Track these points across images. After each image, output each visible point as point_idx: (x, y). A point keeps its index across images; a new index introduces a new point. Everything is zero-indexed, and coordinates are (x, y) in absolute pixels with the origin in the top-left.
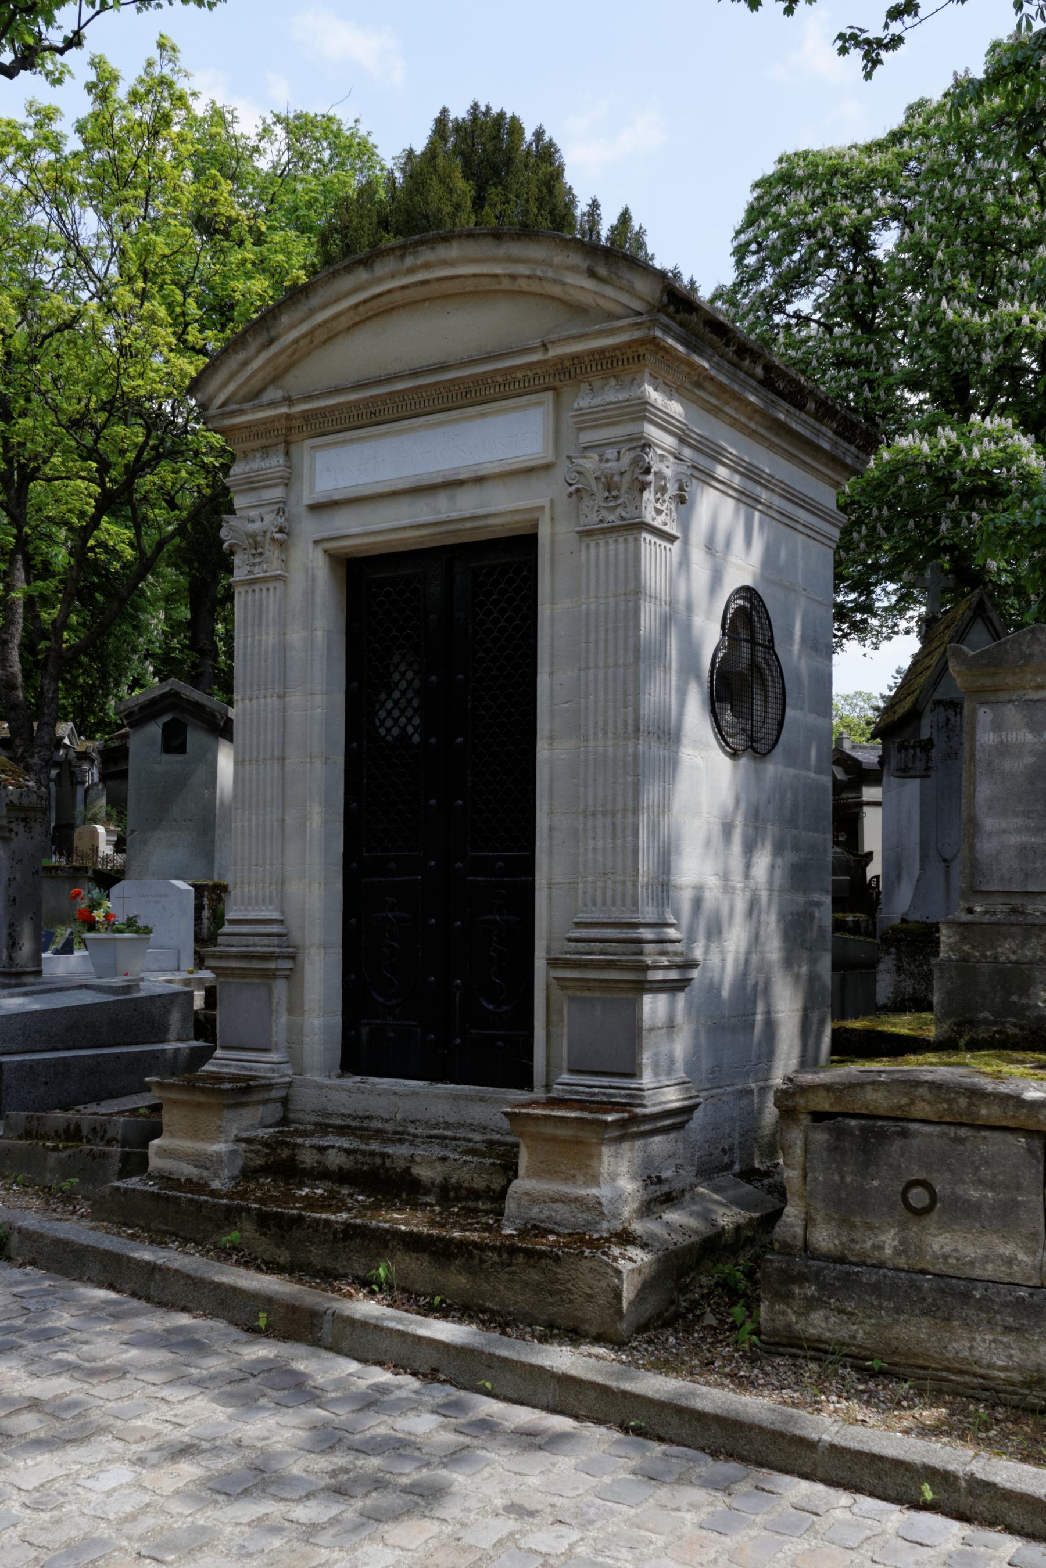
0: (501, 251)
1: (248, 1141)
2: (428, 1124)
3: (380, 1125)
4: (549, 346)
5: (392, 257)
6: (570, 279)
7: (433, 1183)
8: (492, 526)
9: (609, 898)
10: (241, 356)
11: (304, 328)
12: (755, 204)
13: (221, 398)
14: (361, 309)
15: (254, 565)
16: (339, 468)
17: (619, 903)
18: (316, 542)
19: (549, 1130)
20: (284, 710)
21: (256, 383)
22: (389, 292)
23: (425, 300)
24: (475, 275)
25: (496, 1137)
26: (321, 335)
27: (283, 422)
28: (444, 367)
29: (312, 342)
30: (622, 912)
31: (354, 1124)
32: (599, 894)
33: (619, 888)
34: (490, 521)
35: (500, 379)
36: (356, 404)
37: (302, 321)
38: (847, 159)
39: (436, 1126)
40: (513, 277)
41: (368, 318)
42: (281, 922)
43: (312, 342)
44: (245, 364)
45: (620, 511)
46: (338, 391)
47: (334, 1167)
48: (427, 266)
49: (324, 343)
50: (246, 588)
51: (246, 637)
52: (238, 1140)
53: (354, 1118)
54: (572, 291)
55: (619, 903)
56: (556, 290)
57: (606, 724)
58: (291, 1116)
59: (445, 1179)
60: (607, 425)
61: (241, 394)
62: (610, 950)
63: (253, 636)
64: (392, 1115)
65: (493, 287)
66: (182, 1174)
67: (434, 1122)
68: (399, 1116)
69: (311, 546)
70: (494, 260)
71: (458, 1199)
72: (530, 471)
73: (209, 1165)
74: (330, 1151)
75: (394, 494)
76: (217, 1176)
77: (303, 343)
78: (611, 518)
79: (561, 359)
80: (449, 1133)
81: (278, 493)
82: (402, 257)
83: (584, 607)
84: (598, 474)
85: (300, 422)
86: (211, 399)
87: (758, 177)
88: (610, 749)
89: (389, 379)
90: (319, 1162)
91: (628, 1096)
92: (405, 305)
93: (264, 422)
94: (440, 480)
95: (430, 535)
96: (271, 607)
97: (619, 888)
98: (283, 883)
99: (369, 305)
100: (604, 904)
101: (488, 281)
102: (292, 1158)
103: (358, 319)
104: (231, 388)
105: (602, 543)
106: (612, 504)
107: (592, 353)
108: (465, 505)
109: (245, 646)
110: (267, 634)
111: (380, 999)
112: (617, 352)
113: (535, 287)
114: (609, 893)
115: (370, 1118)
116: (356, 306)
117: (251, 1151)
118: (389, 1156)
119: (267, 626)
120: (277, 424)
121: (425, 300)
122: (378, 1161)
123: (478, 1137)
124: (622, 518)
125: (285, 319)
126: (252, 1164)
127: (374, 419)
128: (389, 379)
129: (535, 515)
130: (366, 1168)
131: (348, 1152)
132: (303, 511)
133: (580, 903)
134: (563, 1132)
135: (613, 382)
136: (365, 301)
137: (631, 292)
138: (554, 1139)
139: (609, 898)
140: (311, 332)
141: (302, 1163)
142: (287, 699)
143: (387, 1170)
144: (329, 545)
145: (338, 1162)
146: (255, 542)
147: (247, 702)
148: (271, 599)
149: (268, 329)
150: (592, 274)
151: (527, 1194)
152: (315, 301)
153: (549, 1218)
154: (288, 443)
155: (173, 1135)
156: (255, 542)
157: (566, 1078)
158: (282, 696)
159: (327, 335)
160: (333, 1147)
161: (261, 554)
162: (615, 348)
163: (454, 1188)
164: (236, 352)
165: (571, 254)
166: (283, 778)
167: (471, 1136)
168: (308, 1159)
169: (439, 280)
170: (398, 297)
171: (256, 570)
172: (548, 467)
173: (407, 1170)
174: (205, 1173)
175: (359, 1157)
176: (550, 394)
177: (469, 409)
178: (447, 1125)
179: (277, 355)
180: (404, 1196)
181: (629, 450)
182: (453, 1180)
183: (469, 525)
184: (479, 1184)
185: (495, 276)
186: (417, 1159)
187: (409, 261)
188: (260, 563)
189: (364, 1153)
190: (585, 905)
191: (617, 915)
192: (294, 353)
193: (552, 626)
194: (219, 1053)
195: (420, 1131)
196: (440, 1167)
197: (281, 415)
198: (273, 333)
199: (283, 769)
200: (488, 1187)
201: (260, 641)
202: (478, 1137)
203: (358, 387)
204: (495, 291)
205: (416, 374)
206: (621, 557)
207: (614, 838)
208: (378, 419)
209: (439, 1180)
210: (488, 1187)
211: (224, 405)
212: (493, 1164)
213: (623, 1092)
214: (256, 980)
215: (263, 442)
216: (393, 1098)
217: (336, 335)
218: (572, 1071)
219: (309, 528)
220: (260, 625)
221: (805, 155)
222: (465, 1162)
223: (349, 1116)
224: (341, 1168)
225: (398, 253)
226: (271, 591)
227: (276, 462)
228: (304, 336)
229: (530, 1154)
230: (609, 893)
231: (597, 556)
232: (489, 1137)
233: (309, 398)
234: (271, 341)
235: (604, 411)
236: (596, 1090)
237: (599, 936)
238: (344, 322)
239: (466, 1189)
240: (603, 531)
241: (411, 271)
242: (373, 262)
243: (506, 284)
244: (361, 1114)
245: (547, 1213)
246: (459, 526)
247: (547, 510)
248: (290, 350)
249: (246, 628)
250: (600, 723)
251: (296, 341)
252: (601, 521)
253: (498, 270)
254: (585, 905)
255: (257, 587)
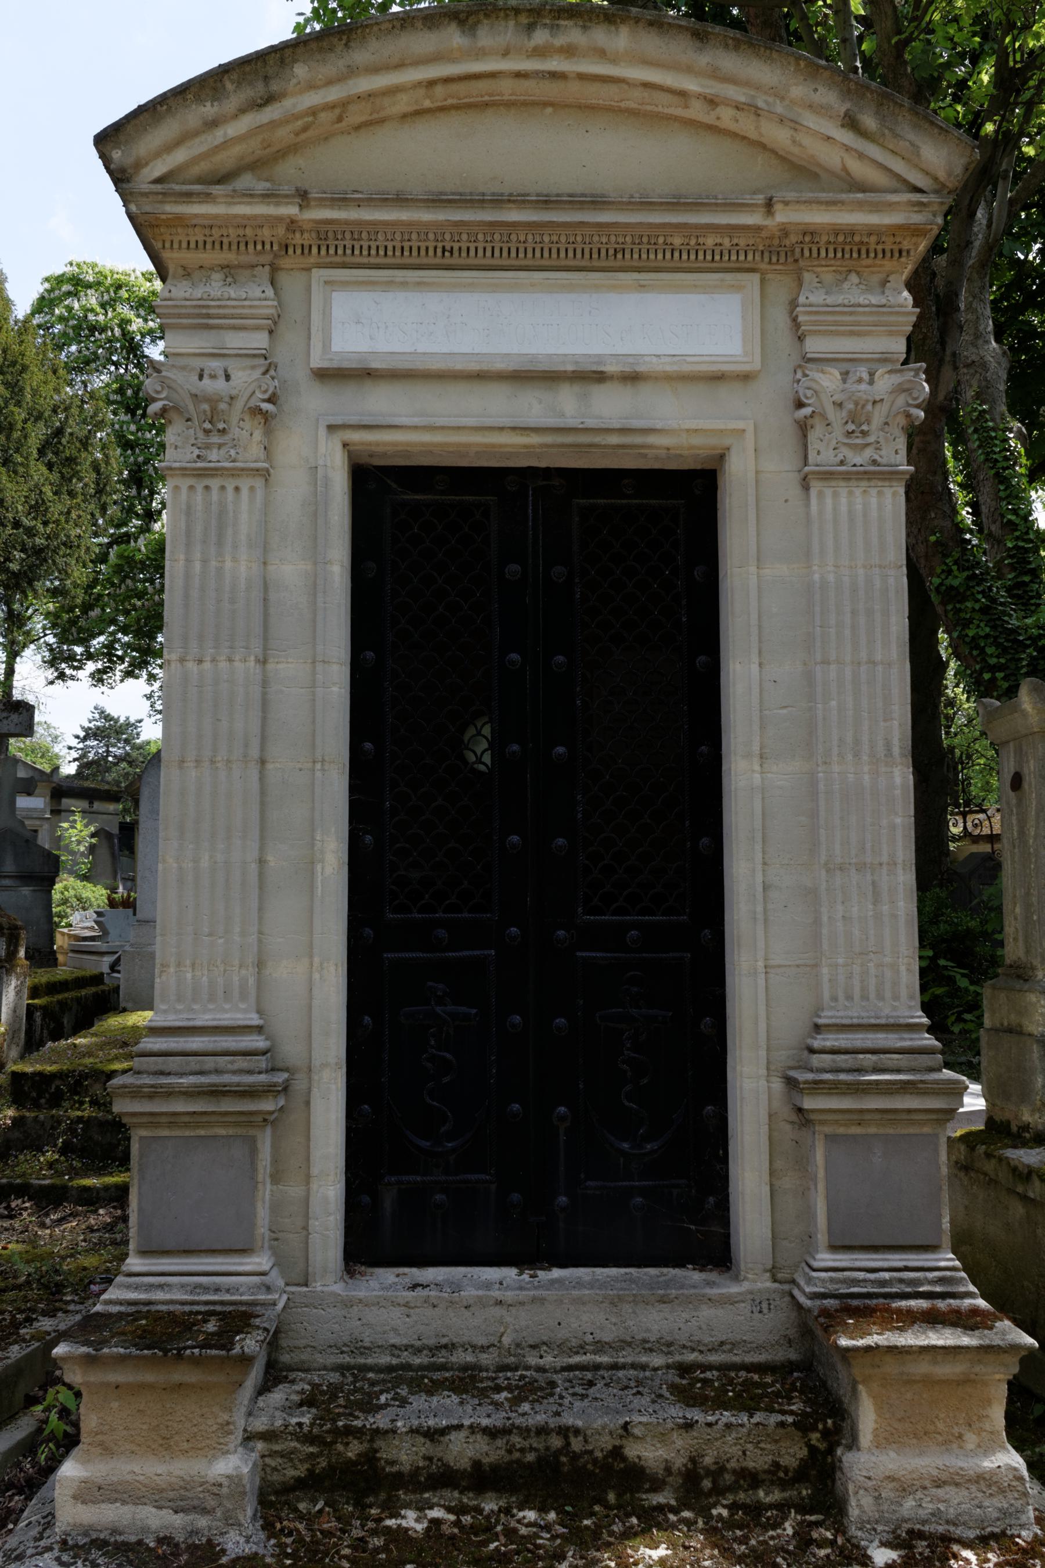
0: (704, 59)
1: (268, 1436)
2: (563, 1348)
3: (470, 1358)
4: (778, 207)
5: (511, 23)
6: (811, 121)
7: (668, 1470)
8: (650, 447)
9: (872, 988)
10: (209, 110)
11: (334, 94)
12: (46, 295)
13: (159, 169)
14: (439, 90)
15: (208, 447)
16: (371, 320)
17: (888, 994)
18: (331, 428)
19: (923, 1367)
20: (265, 683)
21: (227, 159)
22: (493, 75)
23: (546, 104)
24: (646, 85)
25: (691, 1357)
26: (356, 115)
27: (281, 231)
28: (597, 202)
29: (340, 119)
30: (895, 1008)
31: (417, 1361)
32: (856, 982)
33: (888, 974)
34: (652, 439)
35: (677, 241)
36: (423, 229)
37: (329, 83)
38: (132, 278)
39: (581, 1349)
40: (712, 102)
41: (442, 109)
42: (259, 1029)
43: (340, 119)
44: (213, 124)
45: (868, 453)
46: (400, 200)
47: (464, 1464)
48: (569, 51)
49: (358, 128)
50: (191, 481)
51: (188, 561)
52: (249, 1438)
53: (418, 1351)
54: (807, 141)
55: (888, 994)
56: (779, 136)
57: (857, 742)
58: (285, 1358)
59: (692, 1460)
60: (852, 333)
61: (195, 171)
62: (890, 1064)
63: (205, 561)
64: (494, 1340)
65: (671, 111)
66: (146, 1530)
67: (574, 1342)
68: (506, 1340)
69: (322, 432)
70: (689, 70)
71: (719, 1491)
72: (717, 378)
73: (211, 1503)
74: (453, 1436)
75: (481, 377)
76: (231, 1521)
77: (323, 116)
78: (858, 460)
79: (784, 231)
80: (604, 1359)
81: (259, 341)
82: (531, 28)
83: (816, 577)
84: (838, 398)
85: (308, 239)
86: (139, 165)
87: (47, 274)
88: (866, 777)
89: (498, 201)
90: (430, 1459)
91: (941, 1281)
92: (509, 105)
93: (243, 222)
94: (570, 368)
95: (542, 446)
96: (244, 517)
97: (888, 974)
98: (260, 965)
99: (454, 87)
100: (865, 997)
101: (666, 98)
102: (370, 1457)
103: (427, 104)
104: (180, 156)
105: (858, 492)
106: (859, 441)
107: (836, 231)
108: (609, 407)
109: (188, 576)
110: (235, 560)
111: (425, 1144)
112: (873, 239)
113: (746, 125)
114: (872, 982)
115: (450, 1347)
116: (431, 83)
117: (272, 1454)
118: (577, 1432)
119: (235, 547)
120: (266, 233)
121: (546, 104)
122: (556, 1442)
123: (657, 1360)
124: (874, 462)
125: (300, 71)
126: (276, 1477)
127: (448, 260)
128: (498, 201)
129: (727, 441)
130: (530, 1457)
131: (492, 1433)
132: (301, 375)
133: (826, 995)
134: (947, 1370)
135: (854, 278)
136: (447, 80)
137: (913, 159)
138: (929, 1382)
139: (872, 988)
140: (344, 104)
141: (392, 1463)
142: (270, 666)
143: (575, 1457)
144: (356, 437)
145: (470, 1453)
146: (214, 409)
147: (191, 665)
148: (245, 507)
149: (266, 79)
150: (851, 123)
151: (891, 1479)
152: (360, 56)
153: (936, 1514)
154: (274, 269)
155: (107, 1451)
156: (214, 409)
157: (825, 1258)
158: (263, 662)
159: (371, 117)
160: (459, 1427)
161: (223, 432)
162: (872, 231)
163: (709, 1473)
164: (199, 100)
165: (822, 90)
166: (263, 792)
167: (644, 1359)
168: (404, 1454)
169: (582, 77)
170: (506, 88)
171: (214, 455)
172: (746, 377)
173: (617, 1452)
174: (202, 1522)
175: (516, 1439)
176: (756, 277)
177: (621, 275)
178: (600, 1346)
179: (273, 125)
180: (611, 1497)
181: (890, 372)
182: (708, 1460)
183: (614, 440)
184: (758, 1461)
185: (682, 94)
186: (637, 1431)
187: (541, 37)
188: (220, 446)
189: (525, 1432)
190: (834, 999)
191: (887, 1011)
192: (305, 129)
193: (759, 598)
194: (134, 1263)
195: (548, 1360)
196: (680, 1441)
197: (279, 219)
198: (275, 87)
199: (262, 778)
200: (776, 1465)
201: (220, 571)
202: (657, 1360)
203: (437, 201)
204: (676, 119)
205: (547, 202)
206: (874, 514)
207: (876, 902)
208: (455, 261)
209: (680, 1463)
210: (776, 1465)
211: (158, 181)
212: (782, 1424)
213: (931, 1275)
214: (222, 1132)
215: (229, 257)
216: (498, 1311)
217: (382, 121)
218: (834, 1248)
219: (314, 403)
220: (220, 543)
221: (94, 266)
222: (728, 1426)
223: (407, 1348)
224: (477, 1464)
225: (524, 20)
226: (245, 492)
227: (255, 293)
228: (330, 107)
229: (879, 1409)
230: (872, 982)
231: (835, 509)
232: (678, 1358)
233: (342, 201)
234: (269, 99)
235: (851, 313)
236: (886, 1275)
237: (869, 1044)
238: (403, 104)
239: (734, 1472)
240: (847, 477)
241: (540, 52)
242: (478, 22)
243: (697, 111)
244: (432, 1342)
245: (930, 1507)
246: (598, 439)
247: (750, 436)
248: (299, 123)
249: (188, 545)
250: (849, 738)
251: (313, 112)
252: (842, 463)
253: (692, 85)
254: (834, 999)
255: (215, 483)
